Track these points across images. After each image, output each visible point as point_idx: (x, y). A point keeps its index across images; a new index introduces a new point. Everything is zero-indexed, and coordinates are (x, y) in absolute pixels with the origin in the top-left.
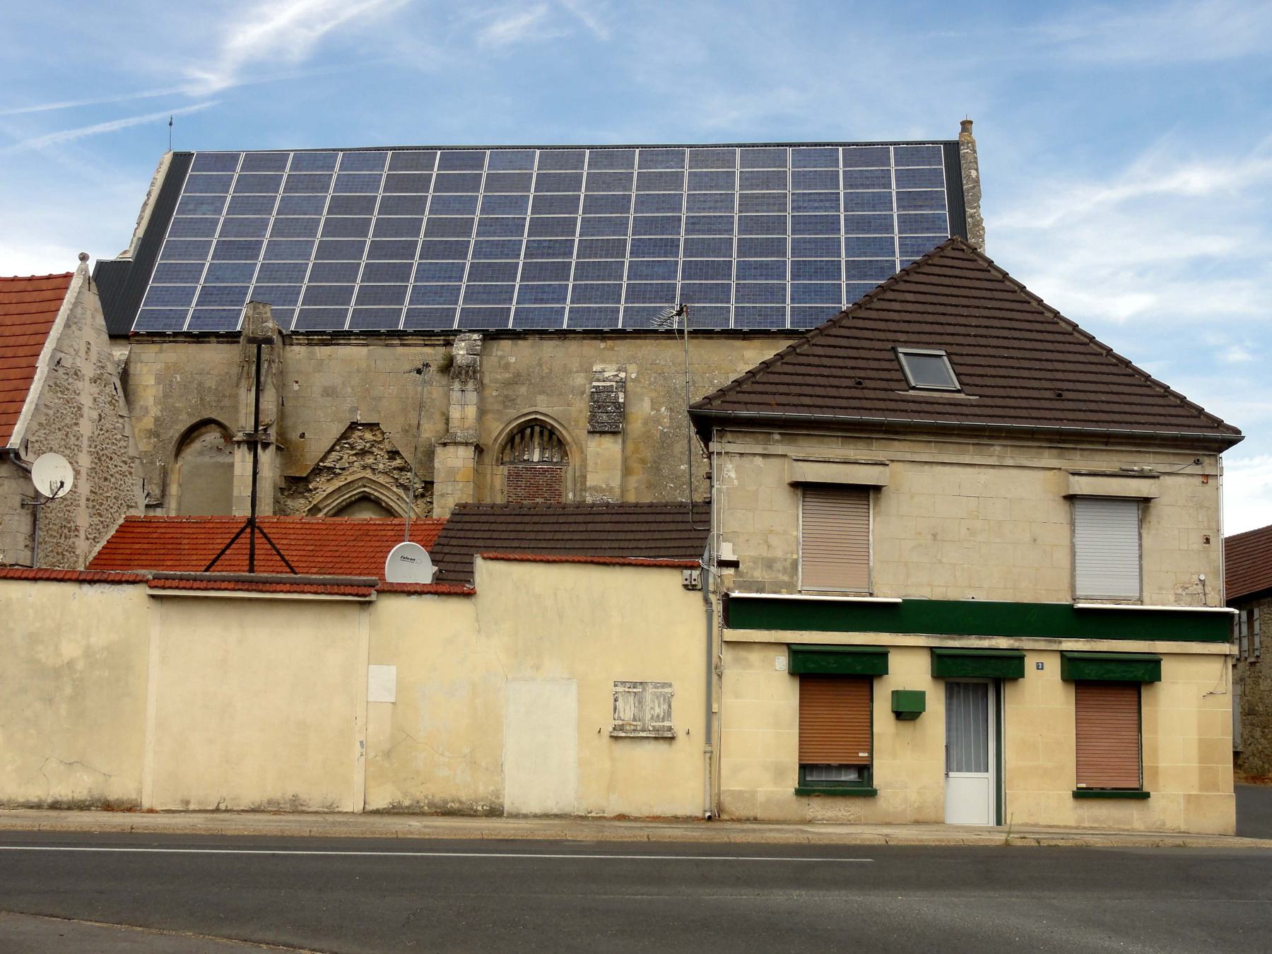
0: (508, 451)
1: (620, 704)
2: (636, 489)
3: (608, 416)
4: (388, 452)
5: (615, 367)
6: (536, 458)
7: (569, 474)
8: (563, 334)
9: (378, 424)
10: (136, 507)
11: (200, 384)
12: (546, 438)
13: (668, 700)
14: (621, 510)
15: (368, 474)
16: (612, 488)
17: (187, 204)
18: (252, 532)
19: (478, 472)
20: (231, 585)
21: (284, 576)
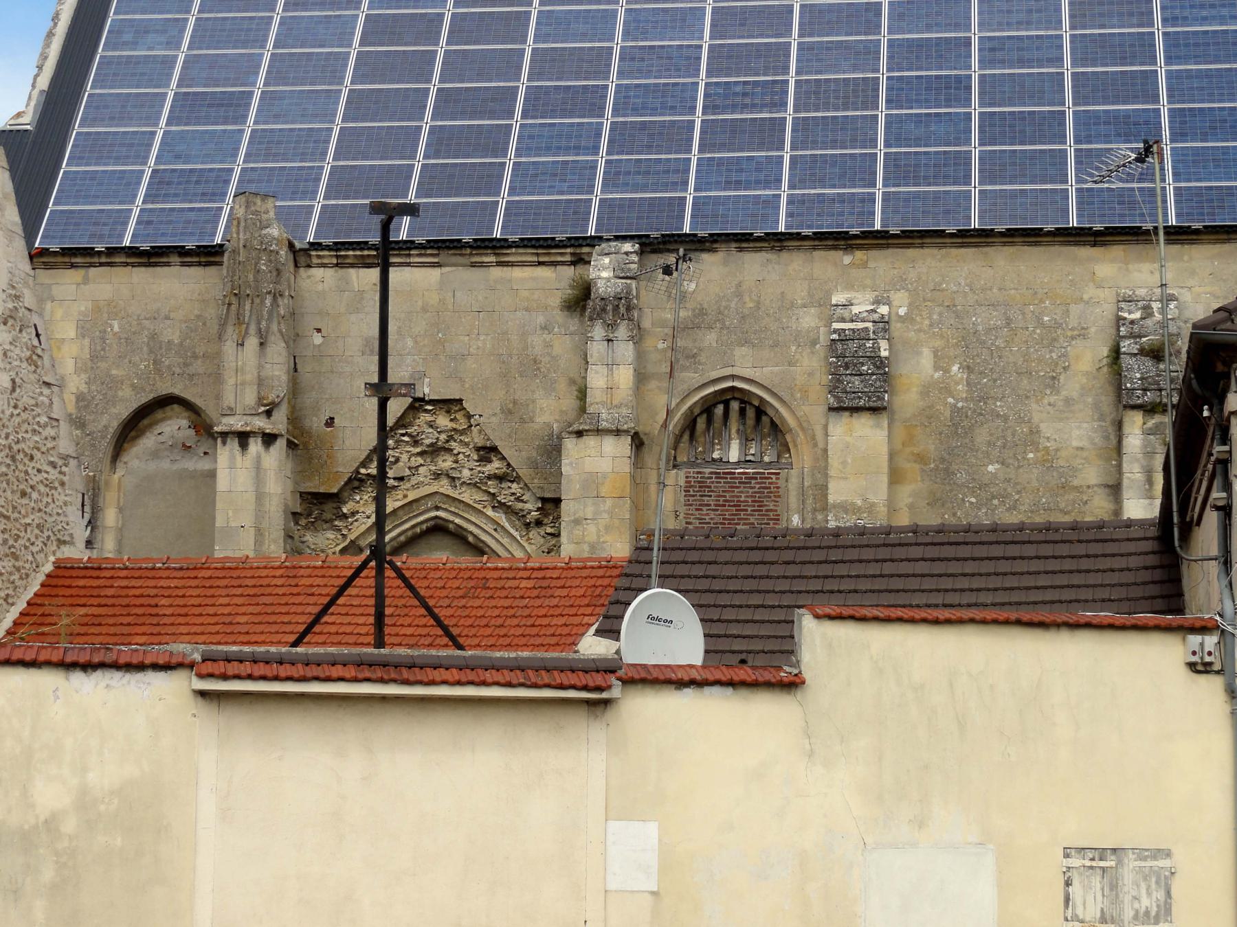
0: (684, 444)
1: (1076, 890)
2: (911, 507)
3: (860, 378)
4: (478, 449)
5: (870, 296)
6: (734, 455)
7: (793, 482)
8: (778, 241)
9: (460, 401)
10: (71, 543)
11: (153, 336)
12: (750, 421)
13: (1165, 881)
14: (940, 538)
15: (444, 486)
16: (873, 505)
17: (120, 32)
18: (380, 570)
19: (637, 482)
20: (351, 672)
21: (443, 653)
